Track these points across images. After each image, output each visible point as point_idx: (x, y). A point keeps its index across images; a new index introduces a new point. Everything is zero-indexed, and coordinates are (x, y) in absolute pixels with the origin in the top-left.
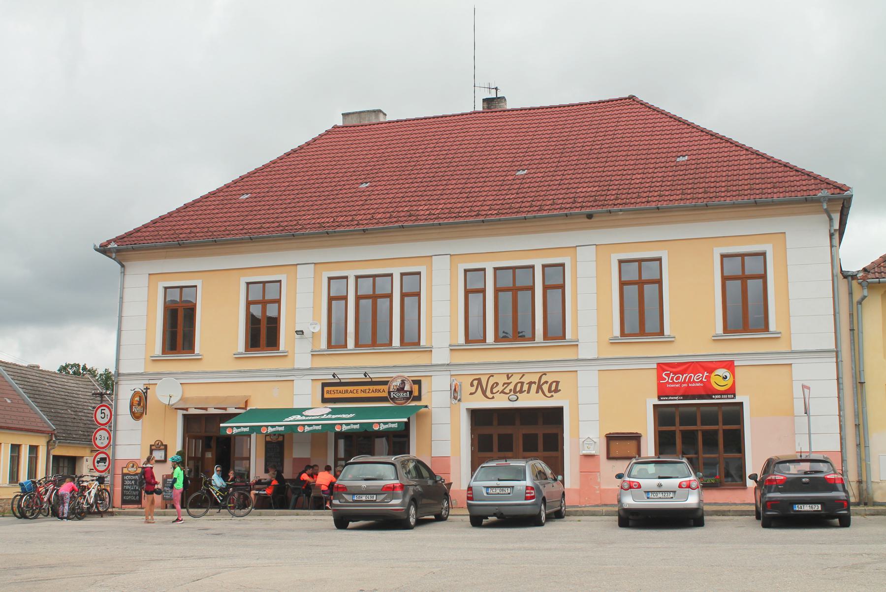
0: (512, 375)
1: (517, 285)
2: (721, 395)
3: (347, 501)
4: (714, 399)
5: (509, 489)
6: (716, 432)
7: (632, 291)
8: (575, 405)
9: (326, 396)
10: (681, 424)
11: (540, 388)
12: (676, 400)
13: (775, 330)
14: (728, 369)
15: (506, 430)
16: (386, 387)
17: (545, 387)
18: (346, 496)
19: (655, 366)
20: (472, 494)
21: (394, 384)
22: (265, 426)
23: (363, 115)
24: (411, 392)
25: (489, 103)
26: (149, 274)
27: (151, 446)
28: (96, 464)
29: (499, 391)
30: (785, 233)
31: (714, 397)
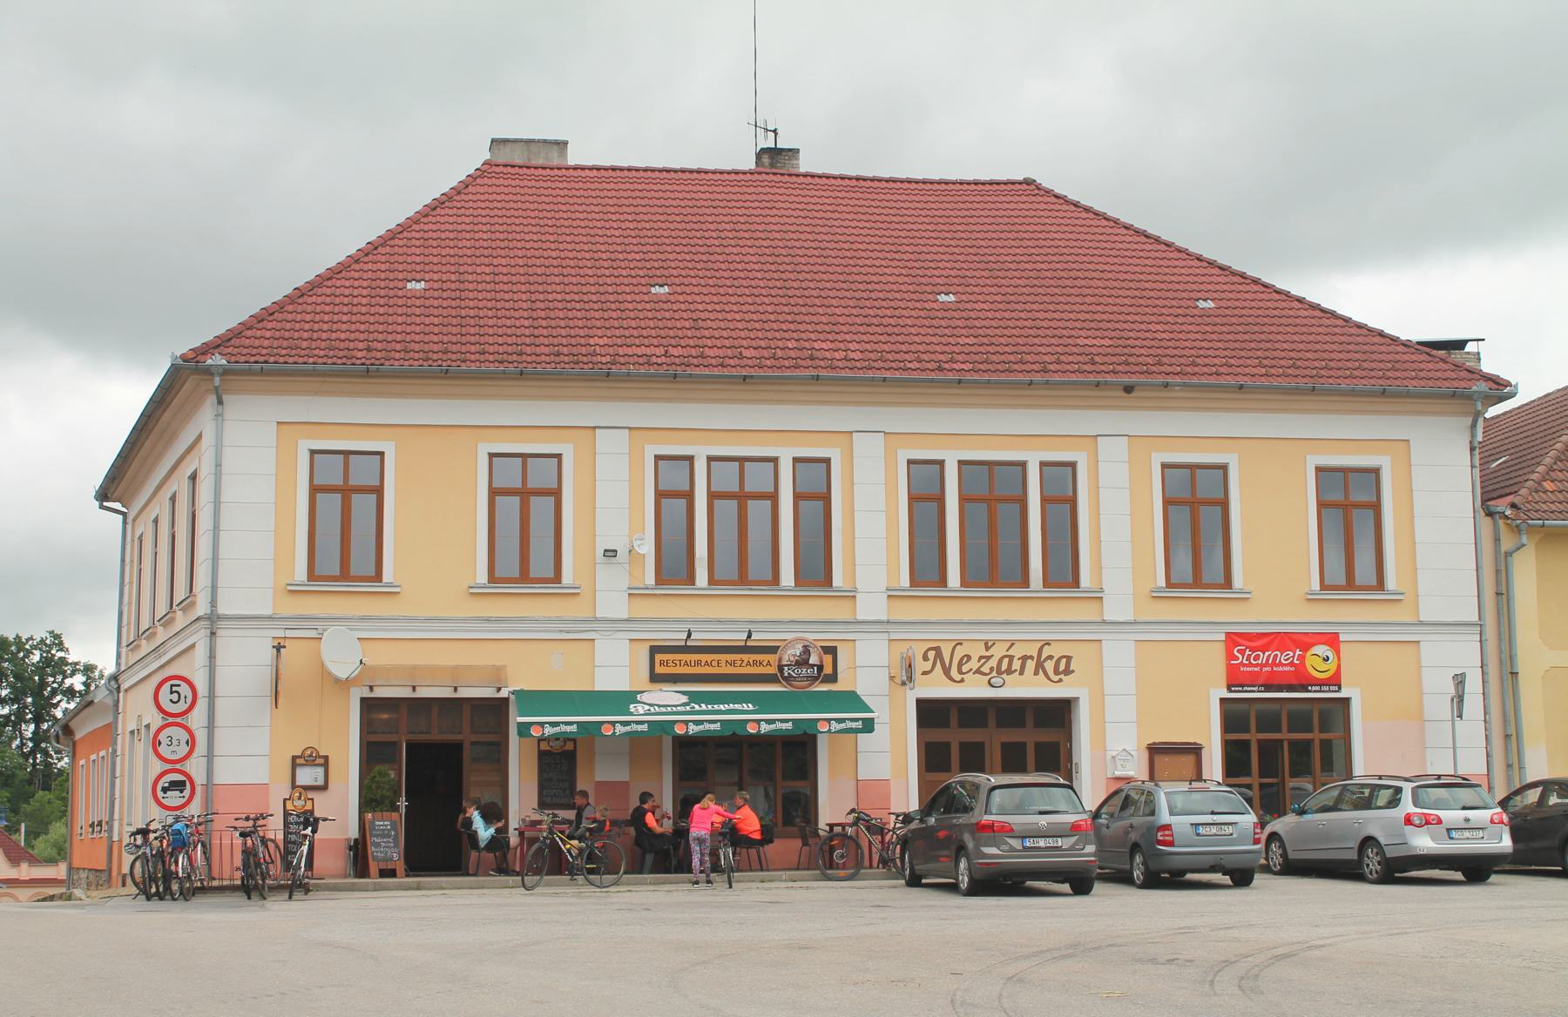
0: (994, 644)
1: (530, 485)
2: (1321, 685)
3: (1012, 849)
4: (1310, 691)
5: (1230, 827)
6: (1309, 743)
7: (1182, 515)
8: (1099, 697)
9: (659, 670)
10: (1258, 731)
11: (1040, 666)
12: (1254, 691)
13: (841, 585)
14: (1330, 645)
15: (973, 735)
16: (773, 658)
17: (1049, 666)
18: (1010, 841)
19: (1223, 637)
20: (1172, 835)
21: (789, 653)
22: (824, 719)
23: (534, 147)
24: (820, 668)
25: (773, 158)
26: (278, 422)
27: (294, 758)
28: (160, 794)
29: (971, 669)
30: (1408, 441)
31: (1310, 688)
